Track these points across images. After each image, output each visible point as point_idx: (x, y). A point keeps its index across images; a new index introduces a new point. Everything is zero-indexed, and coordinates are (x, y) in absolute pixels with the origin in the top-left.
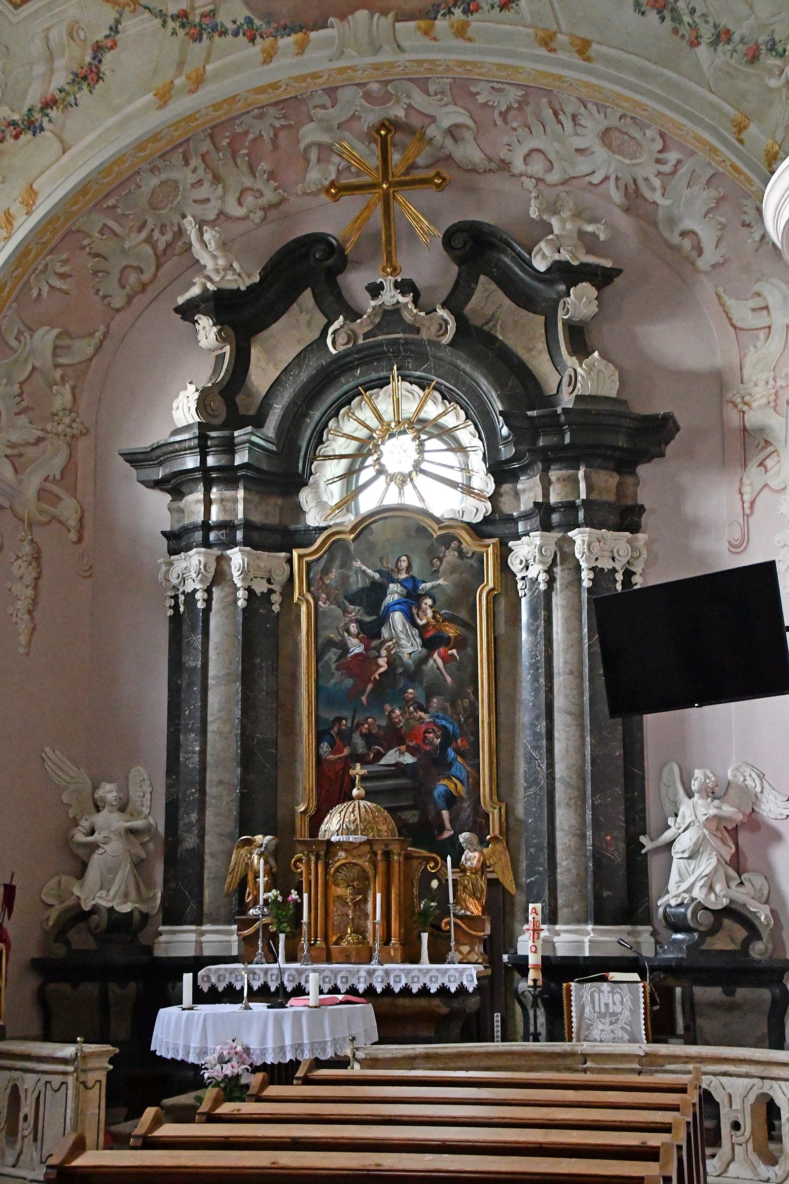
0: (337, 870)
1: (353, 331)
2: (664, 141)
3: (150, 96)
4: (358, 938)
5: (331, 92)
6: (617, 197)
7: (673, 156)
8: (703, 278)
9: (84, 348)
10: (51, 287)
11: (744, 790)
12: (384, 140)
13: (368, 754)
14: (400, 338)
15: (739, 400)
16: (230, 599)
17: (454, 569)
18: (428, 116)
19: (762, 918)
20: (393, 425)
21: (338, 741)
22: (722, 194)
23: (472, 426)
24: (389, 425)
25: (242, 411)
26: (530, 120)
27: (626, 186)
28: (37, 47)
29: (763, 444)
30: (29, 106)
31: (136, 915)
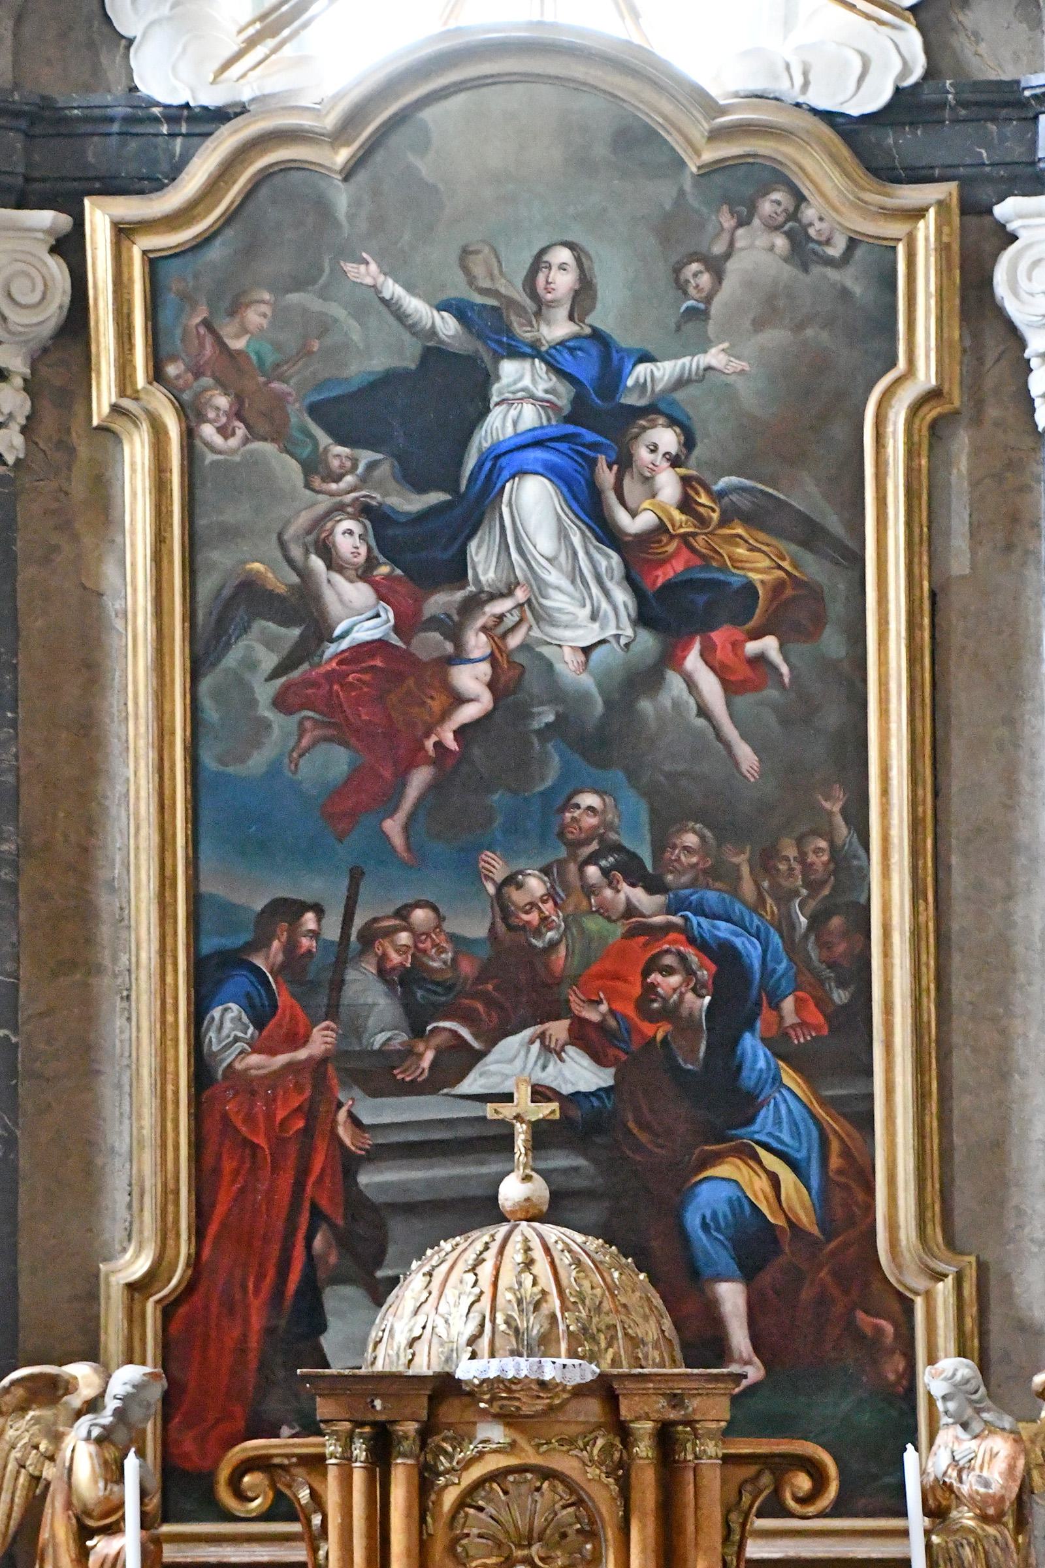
0: (462, 1503)
13: (409, 1054)
21: (284, 999)
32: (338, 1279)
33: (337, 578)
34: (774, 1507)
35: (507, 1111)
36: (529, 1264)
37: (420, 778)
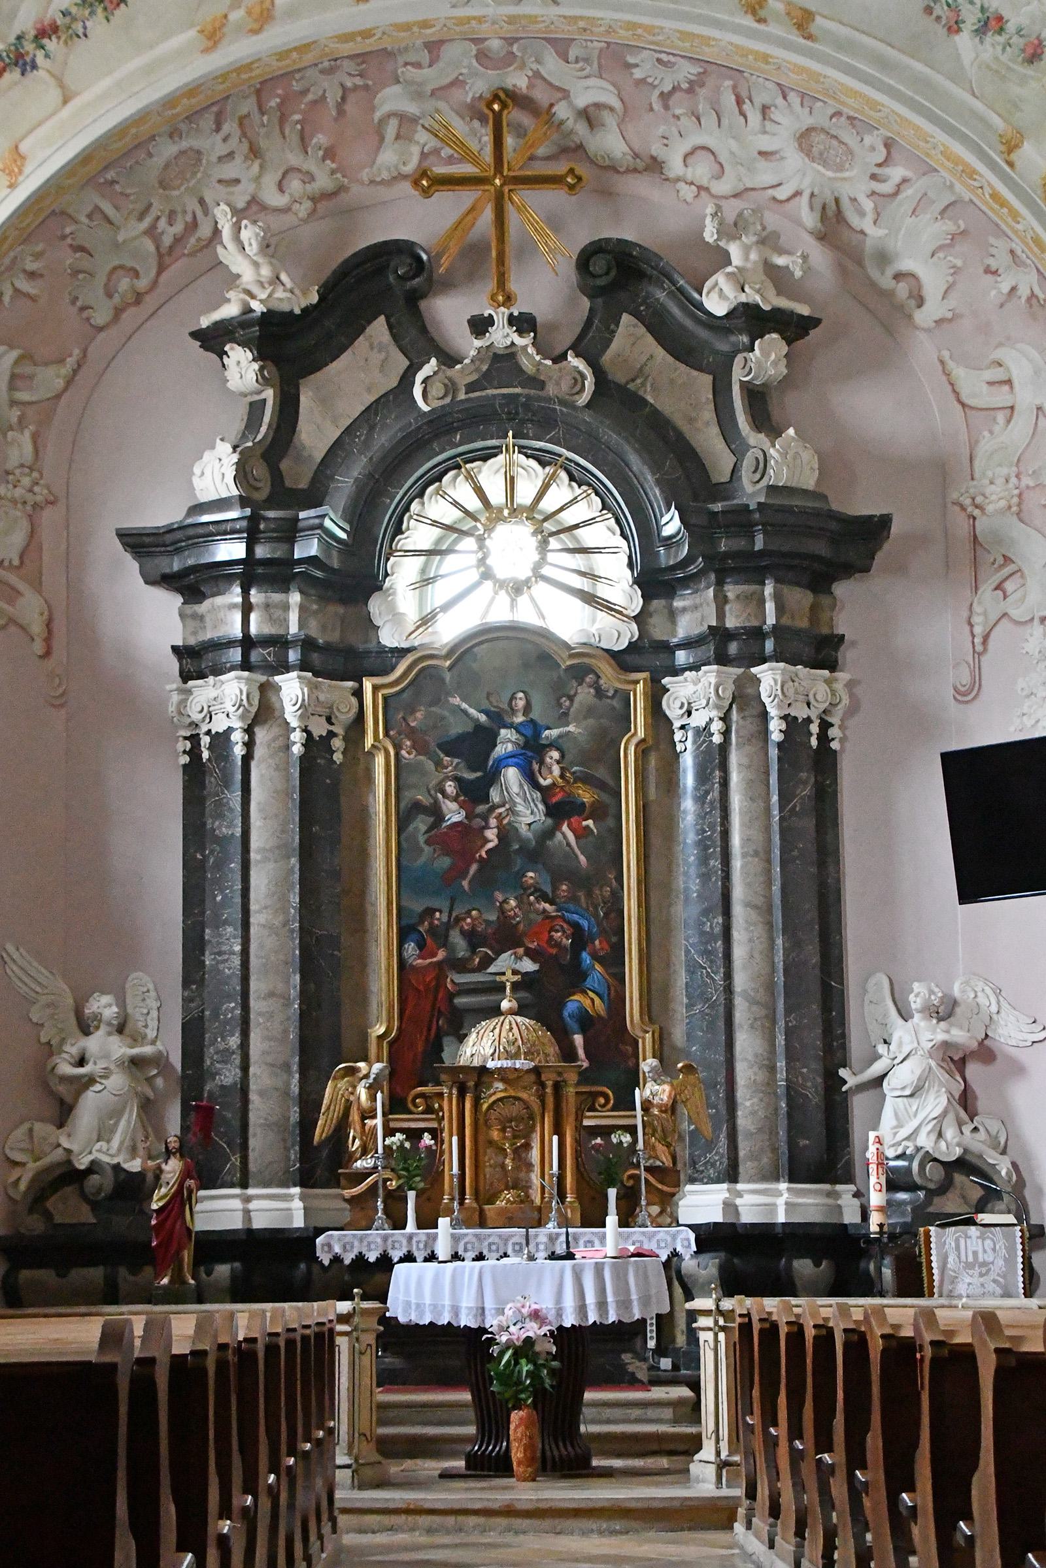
0: (491, 1107)
1: (450, 379)
2: (889, 153)
3: (192, 33)
4: (519, 1196)
5: (434, 47)
6: (810, 219)
7: (896, 173)
8: (922, 336)
10: (17, 290)
13: (471, 959)
14: (518, 395)
15: (968, 502)
16: (280, 742)
17: (590, 712)
18: (559, 89)
19: (1003, 1173)
21: (429, 940)
22: (962, 227)
23: (613, 520)
25: (288, 483)
26: (700, 107)
27: (824, 208)
29: (1000, 560)
30: (19, 32)
32: (448, 1035)
33: (447, 801)
34: (592, 1109)
35: (503, 978)
36: (511, 1029)
37: (474, 868)
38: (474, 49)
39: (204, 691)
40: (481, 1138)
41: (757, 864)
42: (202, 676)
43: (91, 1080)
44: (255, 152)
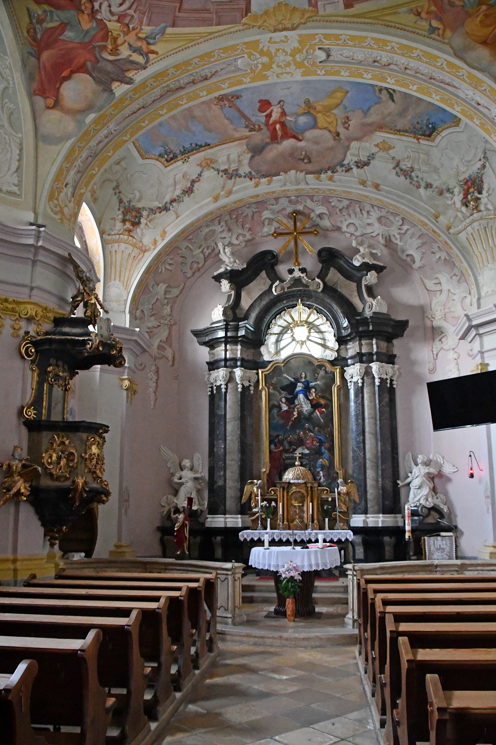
0: (292, 494)
3: (211, 198)
5: (277, 199)
6: (383, 241)
7: (405, 227)
9: (175, 292)
10: (166, 268)
11: (437, 463)
12: (295, 217)
13: (290, 449)
15: (430, 317)
16: (235, 388)
17: (323, 378)
20: (299, 322)
24: (297, 322)
25: (238, 316)
27: (386, 238)
28: (171, 181)
29: (440, 333)
31: (199, 511)
37: (290, 423)
38: (288, 200)
39: (214, 374)
40: (289, 502)
41: (372, 421)
42: (214, 370)
43: (182, 484)
44: (230, 230)
